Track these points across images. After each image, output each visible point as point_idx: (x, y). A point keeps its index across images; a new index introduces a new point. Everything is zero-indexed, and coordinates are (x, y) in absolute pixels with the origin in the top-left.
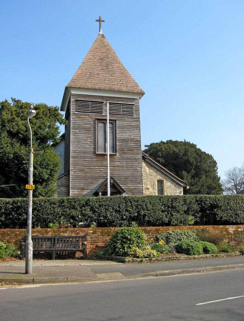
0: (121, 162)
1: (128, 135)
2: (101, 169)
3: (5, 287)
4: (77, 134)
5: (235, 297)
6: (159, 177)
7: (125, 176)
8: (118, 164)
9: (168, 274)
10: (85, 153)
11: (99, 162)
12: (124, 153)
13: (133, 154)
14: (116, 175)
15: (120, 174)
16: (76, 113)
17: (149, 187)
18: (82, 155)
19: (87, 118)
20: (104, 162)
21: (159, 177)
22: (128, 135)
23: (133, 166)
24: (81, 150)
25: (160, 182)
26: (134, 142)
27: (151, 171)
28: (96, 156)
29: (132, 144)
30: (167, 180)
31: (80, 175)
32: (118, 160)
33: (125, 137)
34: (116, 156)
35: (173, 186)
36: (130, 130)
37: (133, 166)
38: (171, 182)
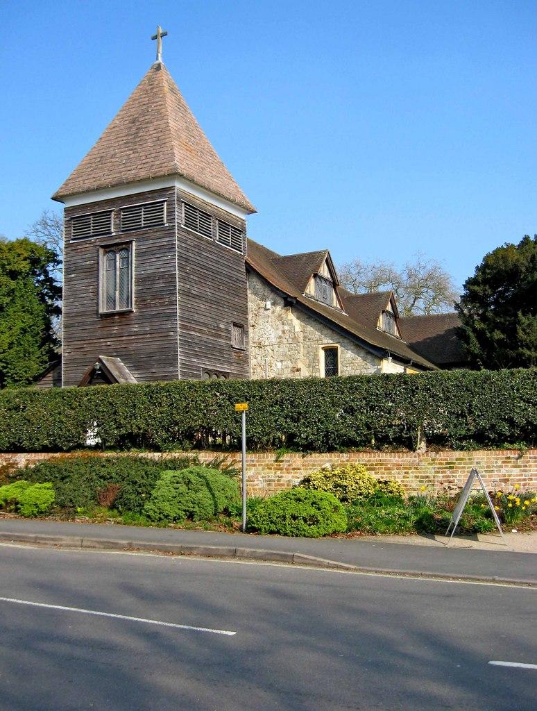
0: (142, 325)
1: (153, 267)
2: (109, 343)
3: (4, 544)
4: (72, 283)
5: (198, 629)
6: (328, 341)
7: (147, 351)
8: (136, 328)
9: (329, 566)
10: (84, 314)
11: (105, 329)
12: (146, 306)
13: (162, 305)
14: (133, 352)
15: (139, 348)
16: (71, 242)
17: (300, 365)
18: (80, 319)
19: (88, 249)
20: (113, 328)
21: (326, 342)
22: (153, 267)
23: (162, 330)
24: (78, 310)
25: (331, 353)
26: (164, 281)
27: (309, 328)
28: (101, 318)
29: (160, 285)
30: (344, 347)
31: (77, 357)
32: (136, 322)
33: (149, 272)
34: (132, 315)
35: (359, 358)
36: (159, 256)
37: (162, 330)
38: (355, 351)
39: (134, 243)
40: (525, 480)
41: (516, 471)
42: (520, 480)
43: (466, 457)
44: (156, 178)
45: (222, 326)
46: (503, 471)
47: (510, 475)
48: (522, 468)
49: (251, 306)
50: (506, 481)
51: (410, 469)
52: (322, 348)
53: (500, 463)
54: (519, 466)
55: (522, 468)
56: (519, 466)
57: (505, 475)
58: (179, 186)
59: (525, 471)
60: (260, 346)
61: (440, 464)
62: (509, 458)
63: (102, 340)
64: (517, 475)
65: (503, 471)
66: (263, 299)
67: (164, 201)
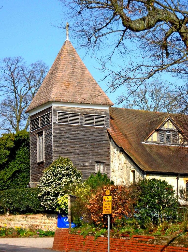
28: (38, 165)
39: (44, 132)
40: (27, 224)
41: (25, 222)
42: (26, 225)
43: (14, 217)
44: (46, 104)
45: (87, 164)
46: (22, 222)
47: (23, 223)
48: (27, 221)
49: (111, 152)
50: (22, 225)
51: (2, 221)
52: (131, 171)
53: (21, 219)
54: (26, 220)
55: (27, 221)
56: (26, 220)
57: (22, 223)
58: (54, 106)
59: (27, 222)
60: (114, 171)
61: (9, 219)
62: (24, 217)
63: (38, 175)
64: (25, 223)
65: (22, 222)
66: (115, 148)
67: (49, 113)
